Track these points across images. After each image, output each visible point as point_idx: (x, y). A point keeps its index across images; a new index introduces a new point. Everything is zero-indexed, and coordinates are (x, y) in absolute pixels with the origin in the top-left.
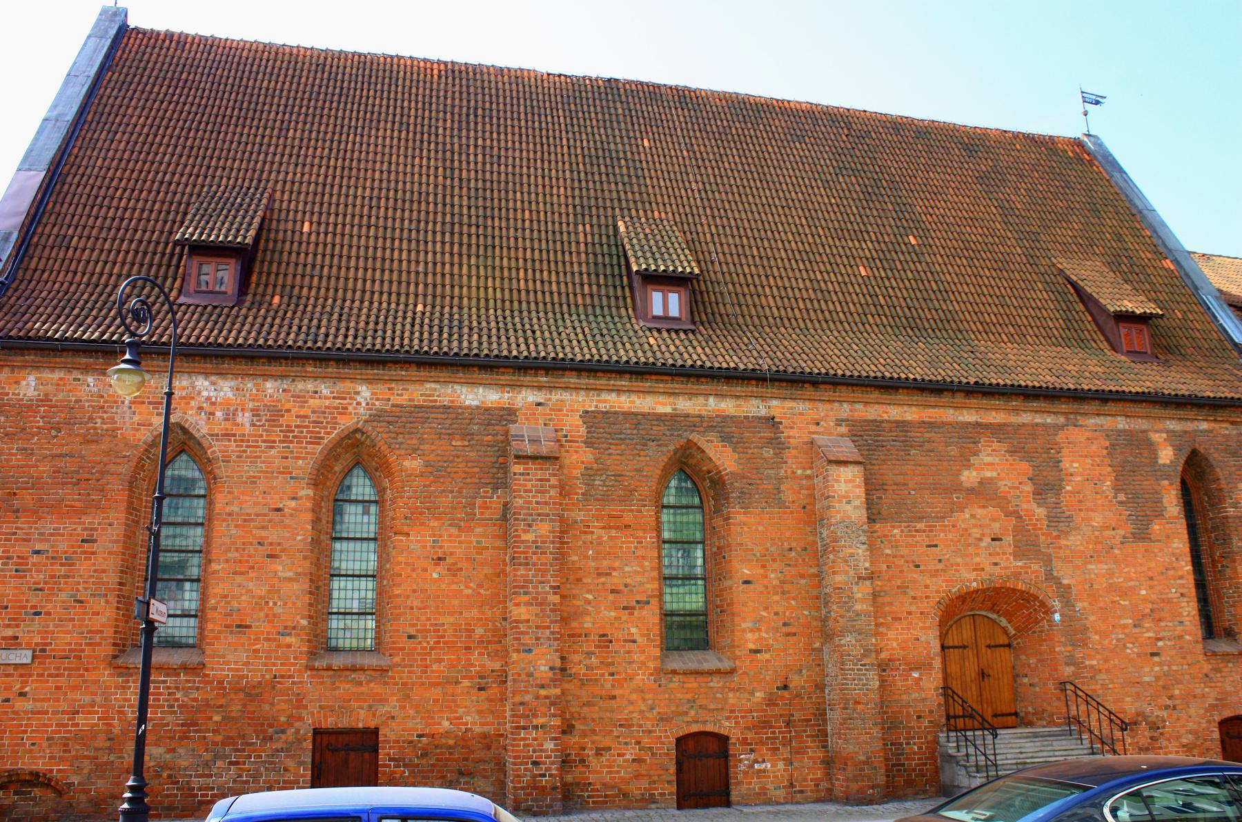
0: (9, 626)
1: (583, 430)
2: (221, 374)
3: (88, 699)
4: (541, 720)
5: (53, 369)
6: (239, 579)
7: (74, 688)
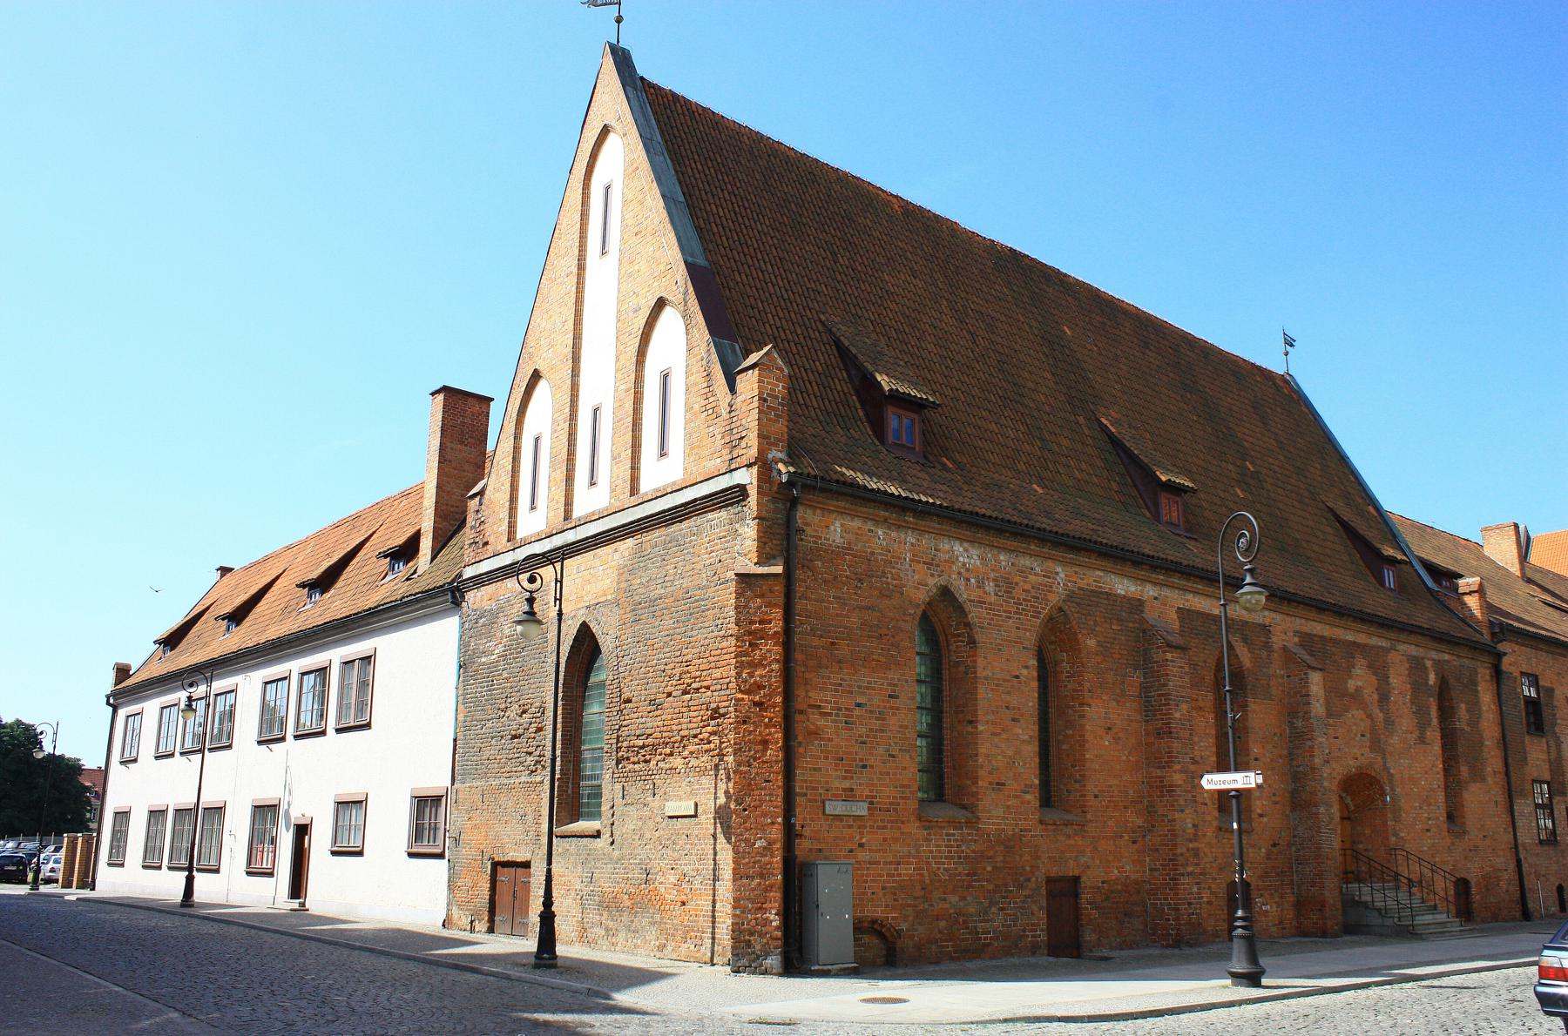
1: (1176, 625)
3: (905, 849)
4: (1190, 869)
5: (853, 517)
6: (996, 739)
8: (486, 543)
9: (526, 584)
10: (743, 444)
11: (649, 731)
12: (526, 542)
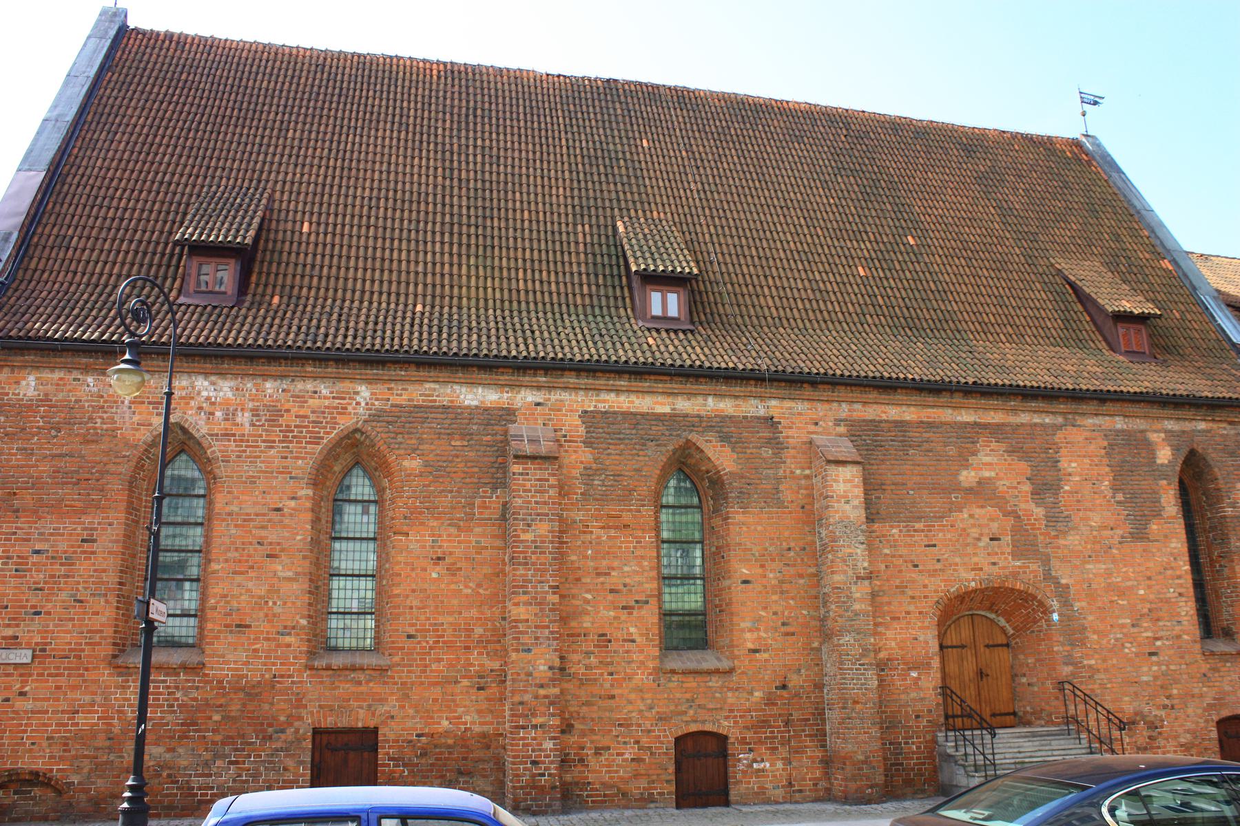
0: (9, 626)
1: (582, 430)
2: (222, 374)
3: (88, 698)
5: (53, 369)
6: (239, 578)
7: (74, 688)
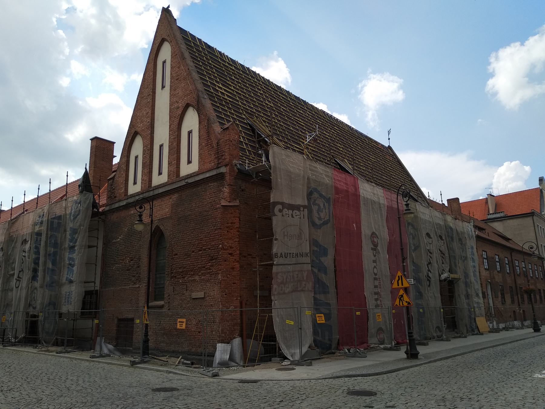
8: (115, 197)
9: (138, 210)
10: (223, 158)
11: (184, 266)
12: (133, 196)
